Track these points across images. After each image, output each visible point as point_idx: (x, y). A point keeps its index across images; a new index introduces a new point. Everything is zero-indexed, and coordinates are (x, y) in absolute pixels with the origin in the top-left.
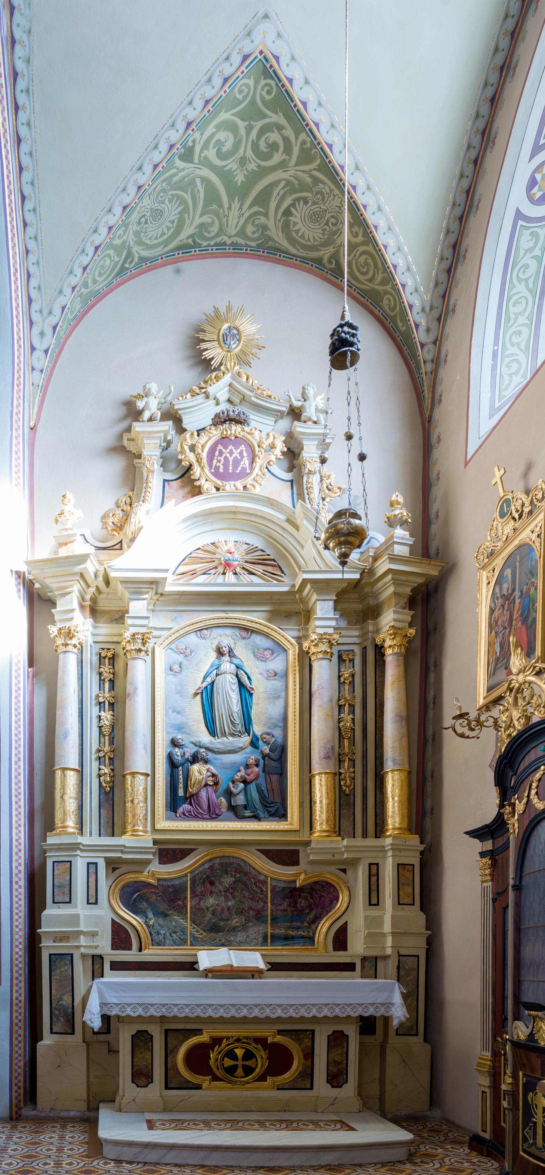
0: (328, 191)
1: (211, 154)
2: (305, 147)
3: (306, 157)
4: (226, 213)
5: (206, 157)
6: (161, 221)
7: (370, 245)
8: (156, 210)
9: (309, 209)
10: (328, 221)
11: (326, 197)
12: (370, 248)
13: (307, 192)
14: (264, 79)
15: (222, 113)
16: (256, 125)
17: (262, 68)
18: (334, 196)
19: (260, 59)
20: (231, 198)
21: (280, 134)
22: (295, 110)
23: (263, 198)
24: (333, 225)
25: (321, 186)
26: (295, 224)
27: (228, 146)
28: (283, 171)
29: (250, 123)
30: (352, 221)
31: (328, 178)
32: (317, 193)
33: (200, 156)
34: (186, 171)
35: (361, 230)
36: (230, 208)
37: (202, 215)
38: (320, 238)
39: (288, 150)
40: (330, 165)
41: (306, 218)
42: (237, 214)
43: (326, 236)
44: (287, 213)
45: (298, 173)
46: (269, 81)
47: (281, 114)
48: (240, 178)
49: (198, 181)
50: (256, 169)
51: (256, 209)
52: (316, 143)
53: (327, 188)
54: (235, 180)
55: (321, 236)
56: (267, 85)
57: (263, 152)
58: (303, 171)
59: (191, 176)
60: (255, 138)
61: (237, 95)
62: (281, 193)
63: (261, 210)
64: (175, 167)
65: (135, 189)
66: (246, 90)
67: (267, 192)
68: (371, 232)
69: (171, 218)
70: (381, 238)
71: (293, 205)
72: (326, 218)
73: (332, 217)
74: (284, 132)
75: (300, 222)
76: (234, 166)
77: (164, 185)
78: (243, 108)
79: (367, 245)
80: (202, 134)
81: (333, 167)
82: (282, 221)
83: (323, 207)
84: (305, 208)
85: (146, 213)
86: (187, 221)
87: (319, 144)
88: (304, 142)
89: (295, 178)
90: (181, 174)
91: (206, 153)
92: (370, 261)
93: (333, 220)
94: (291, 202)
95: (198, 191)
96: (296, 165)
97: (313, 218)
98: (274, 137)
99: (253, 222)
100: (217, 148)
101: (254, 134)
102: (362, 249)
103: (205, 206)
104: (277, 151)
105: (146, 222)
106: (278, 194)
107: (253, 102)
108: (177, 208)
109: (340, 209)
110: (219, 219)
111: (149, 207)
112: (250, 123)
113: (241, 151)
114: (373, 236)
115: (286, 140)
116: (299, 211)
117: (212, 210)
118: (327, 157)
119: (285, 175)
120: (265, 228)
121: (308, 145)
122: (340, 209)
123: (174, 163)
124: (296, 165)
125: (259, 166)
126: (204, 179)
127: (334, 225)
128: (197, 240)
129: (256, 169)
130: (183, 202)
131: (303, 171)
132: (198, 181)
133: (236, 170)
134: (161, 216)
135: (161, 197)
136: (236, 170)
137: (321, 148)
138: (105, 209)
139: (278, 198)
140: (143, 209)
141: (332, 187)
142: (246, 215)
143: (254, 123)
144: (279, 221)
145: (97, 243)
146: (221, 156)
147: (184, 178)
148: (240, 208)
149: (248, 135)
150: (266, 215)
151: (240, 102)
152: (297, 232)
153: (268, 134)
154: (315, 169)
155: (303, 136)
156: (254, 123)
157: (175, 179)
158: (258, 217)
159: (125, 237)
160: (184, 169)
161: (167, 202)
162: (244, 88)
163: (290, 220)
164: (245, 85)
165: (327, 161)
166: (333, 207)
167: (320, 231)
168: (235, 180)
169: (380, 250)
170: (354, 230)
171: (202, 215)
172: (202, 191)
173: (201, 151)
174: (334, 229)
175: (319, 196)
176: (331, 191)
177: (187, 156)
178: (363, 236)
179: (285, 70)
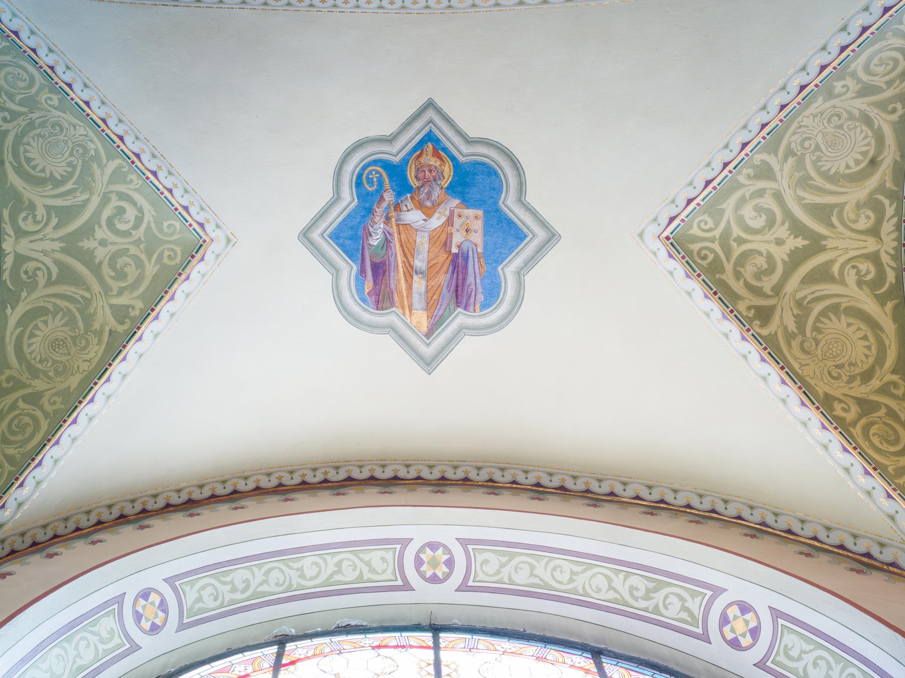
3: (121, 313)
23: (67, 276)
29: (143, 242)
36: (53, 240)
37: (45, 206)
48: (87, 244)
49: (85, 197)
51: (55, 270)
53: (96, 348)
62: (77, 297)
80: (136, 190)
92: (29, 430)
101: (133, 250)
102: (39, 414)
108: (831, 320)
112: (143, 242)
115: (134, 286)
120: (859, 206)
124: (111, 307)
125: (100, 263)
128: (876, 292)
143: (142, 247)
148: (53, 251)
150: (49, 283)
152: (36, 327)
157: (95, 166)
174: (845, 115)
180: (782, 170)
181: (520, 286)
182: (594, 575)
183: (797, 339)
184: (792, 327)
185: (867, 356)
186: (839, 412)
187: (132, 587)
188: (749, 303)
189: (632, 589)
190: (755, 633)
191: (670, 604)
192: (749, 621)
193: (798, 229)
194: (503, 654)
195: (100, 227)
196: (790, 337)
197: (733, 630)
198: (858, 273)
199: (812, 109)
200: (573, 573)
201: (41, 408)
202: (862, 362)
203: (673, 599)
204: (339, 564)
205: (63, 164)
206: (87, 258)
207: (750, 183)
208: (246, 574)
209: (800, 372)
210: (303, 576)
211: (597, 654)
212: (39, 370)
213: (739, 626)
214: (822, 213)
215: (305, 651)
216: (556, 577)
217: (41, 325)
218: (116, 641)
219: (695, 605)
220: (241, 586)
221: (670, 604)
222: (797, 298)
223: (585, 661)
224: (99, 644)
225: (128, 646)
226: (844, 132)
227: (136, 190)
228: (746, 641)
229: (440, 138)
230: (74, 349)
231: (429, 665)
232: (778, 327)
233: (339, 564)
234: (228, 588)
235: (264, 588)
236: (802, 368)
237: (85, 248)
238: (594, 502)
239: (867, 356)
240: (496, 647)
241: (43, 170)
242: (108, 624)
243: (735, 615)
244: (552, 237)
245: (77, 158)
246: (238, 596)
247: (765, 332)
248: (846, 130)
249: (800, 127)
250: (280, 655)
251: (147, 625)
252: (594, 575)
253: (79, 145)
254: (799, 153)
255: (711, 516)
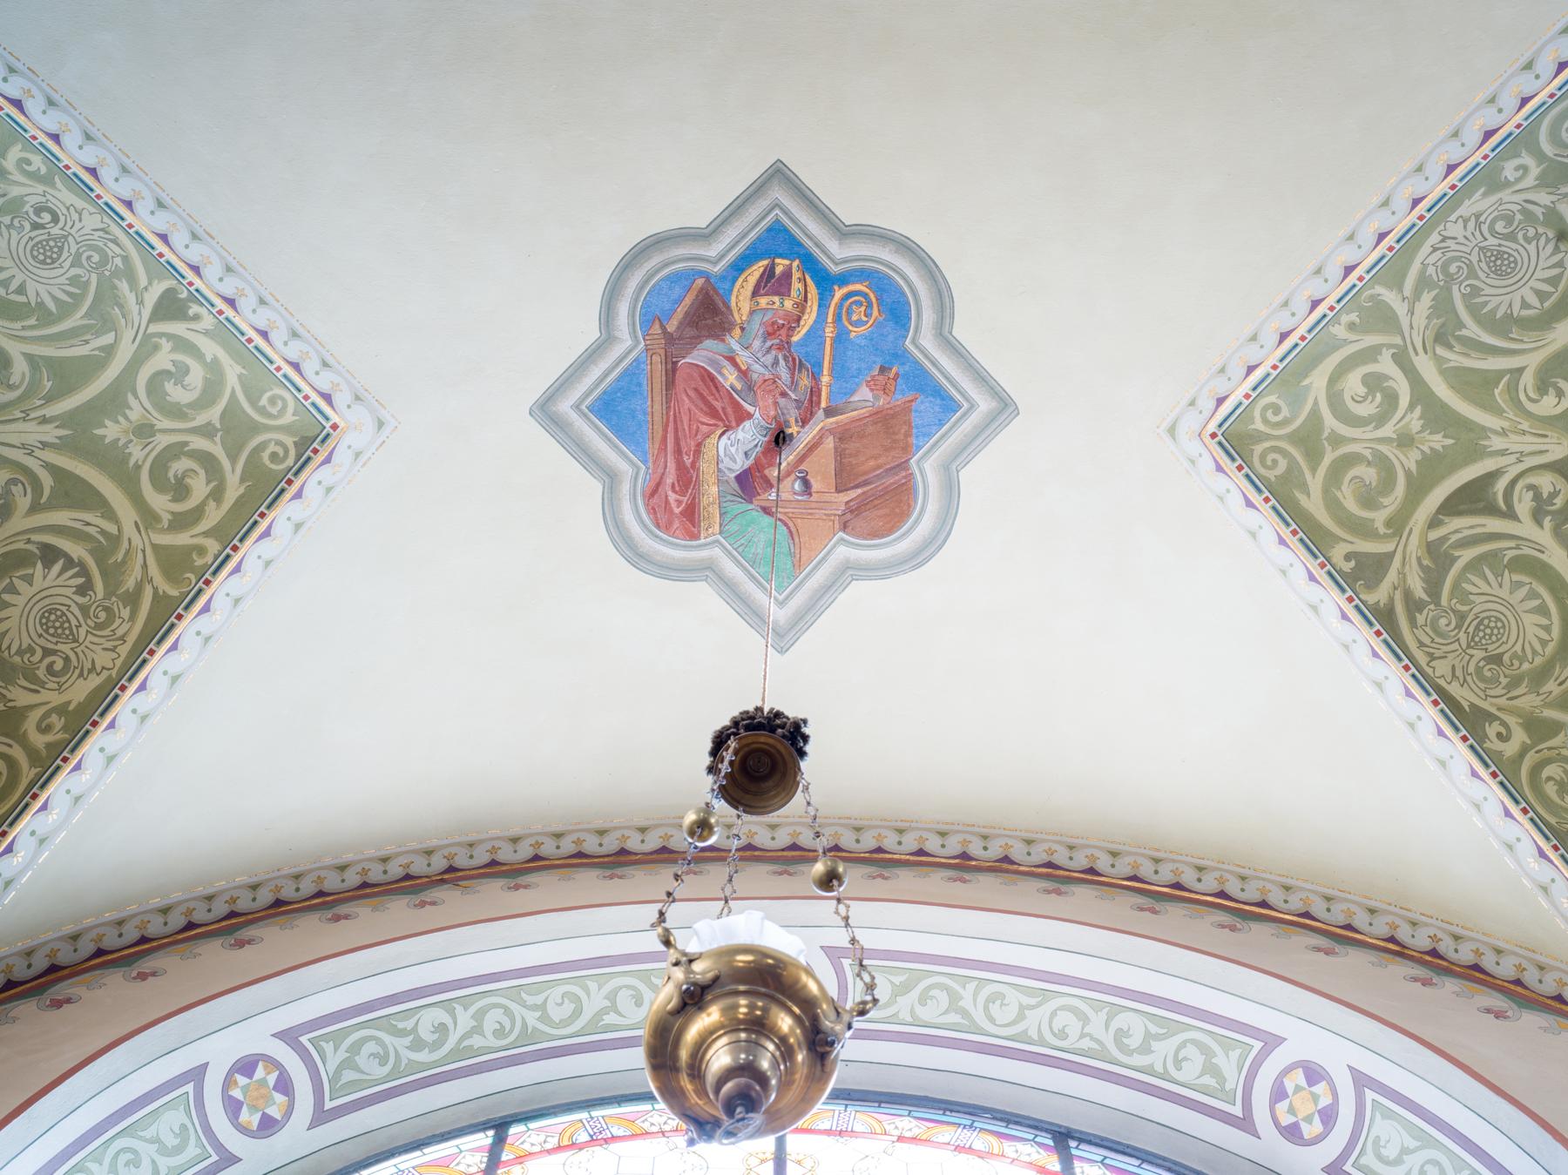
0: (120, 632)
1: (163, 359)
2: (195, 557)
3: (176, 562)
4: (33, 415)
5: (156, 348)
6: (30, 263)
7: (34, 771)
8: (61, 249)
9: (68, 602)
10: (54, 652)
11: (107, 632)
12: (28, 773)
13: (106, 586)
14: (295, 443)
15: (239, 369)
16: (215, 443)
17: (310, 434)
18: (113, 650)
19: (325, 428)
20: (65, 420)
21: (207, 498)
22: (256, 517)
23: (73, 492)
24: (50, 667)
25: (126, 613)
26: (29, 580)
27: (177, 394)
28: (136, 522)
29: (218, 430)
30: (71, 708)
31: (145, 624)
32: (106, 609)
33: (161, 335)
34: (135, 309)
35: (60, 736)
36: (44, 420)
37: (30, 358)
38: (9, 648)
39: (181, 522)
40: (173, 619)
41: (47, 601)
42: (31, 439)
43: (17, 659)
44: (50, 555)
45: (140, 555)
46: (292, 453)
47: (242, 490)
48: (111, 431)
49: (108, 339)
50: (131, 463)
51: (47, 481)
52: (207, 576)
53: (125, 627)
54: (107, 422)
55: (13, 651)
56: (286, 451)
57: (166, 469)
58: (145, 566)
59: (123, 321)
60: (192, 446)
61: (268, 394)
63: (47, 492)
64: (150, 283)
65: (127, 196)
66: (274, 411)
67: (86, 497)
68: (65, 760)
69: (31, 288)
70: (60, 788)
71: (70, 562)
72: (60, 647)
73: (67, 659)
74: (212, 504)
75: (35, 589)
76: (135, 414)
77: (118, 261)
78: (244, 412)
79: (33, 764)
80: (206, 333)
81: (173, 626)
82: (29, 547)
83: (82, 631)
84: (69, 592)
85: (61, 224)
86: (18, 325)
87: (207, 583)
88: (201, 550)
89: (128, 552)
90: (131, 298)
91: (166, 346)
93: (59, 665)
94: (75, 557)
95: (87, 342)
96: (155, 547)
97: (53, 617)
98: (200, 487)
99: (14, 481)
100: (173, 369)
101: (199, 443)
102: (17, 752)
103: (50, 361)
104: (175, 500)
105: (36, 226)
106: (88, 524)
107: (256, 428)
108: (54, 298)
109: (90, 671)
110: (20, 399)
111: (73, 231)
112: (218, 430)
113: (166, 423)
114: (58, 768)
115: (197, 513)
116: (60, 581)
117: (41, 380)
118: (186, 608)
119: (129, 530)
121: (199, 562)
122: (90, 671)
123: (160, 280)
125: (138, 467)
126: (109, 350)
127: (50, 669)
129: (131, 463)
130: (65, 310)
131: (145, 566)
132: (108, 339)
133: (127, 418)
134: (43, 262)
135: (89, 258)
136: (127, 418)
137: (200, 591)
138: (89, 126)
139: (78, 525)
140: (75, 216)
141: (131, 639)
142: (30, 462)
143: (218, 439)
144: (29, 541)
145: (29, 105)
146: (160, 376)
147: (121, 307)
148: (45, 445)
149: (194, 431)
151: (253, 403)
152: (1542, 295)
153: (202, 472)
154: (155, 589)
155: (213, 546)
156: (218, 439)
157: (124, 286)
158: (29, 490)
159: (22, 179)
160: (140, 303)
161: (74, 271)
162: (280, 404)
163: (34, 565)
164: (285, 407)
165: (180, 610)
166: (90, 655)
167: (26, 642)
168: (107, 422)
169: (35, 796)
170: (54, 718)
171: (30, 358)
172: (83, 351)
173: (170, 337)
174: (41, 673)
175: (103, 615)
176: (123, 639)
177: (171, 307)
178: (49, 746)
179: (314, 480)
180: (1413, 314)
181: (951, 490)
182: (1054, 1014)
183: (1425, 612)
184: (1418, 589)
185: (1544, 643)
186: (1494, 744)
187: (220, 1052)
188: (1349, 548)
189: (1120, 1034)
190: (1328, 1116)
191: (1185, 1059)
192: (1319, 1096)
193: (1438, 416)
194: (898, 1141)
195: (1408, 473)
196: (1414, 606)
197: (1292, 1110)
198: (1537, 497)
199: (1466, 209)
200: (1022, 1008)
201: (23, 741)
202: (1534, 652)
203: (1191, 1051)
204: (612, 996)
205: (63, 280)
206: (114, 461)
207: (1354, 337)
208: (440, 1015)
209: (1429, 671)
210: (545, 1019)
211: (1063, 1138)
212: (13, 667)
213: (1303, 1105)
214: (1477, 386)
215: (542, 1137)
216: (992, 1012)
217: (1533, 300)
218: (192, 1151)
219: (1230, 1068)
220: (426, 1033)
221: (1185, 1059)
222: (1429, 540)
223: (1035, 1153)
224: (158, 1158)
225: (215, 1158)
226: (1519, 247)
227: (206, 333)
228: (1311, 1129)
229: (766, 227)
230: (1474, 258)
231: (763, 1161)
232: (1395, 588)
233: (612, 996)
234: (407, 1041)
235: (477, 1041)
236: (1433, 664)
237: (107, 441)
238: (1056, 885)
239: (1544, 643)
240: (887, 1127)
241: (1516, 586)
242: (170, 1122)
243: (1297, 1085)
244: (1005, 406)
245: (88, 271)
246: (423, 1056)
247: (1371, 598)
248: (1522, 242)
249: (1444, 239)
250: (500, 1141)
251: (250, 1118)
252: (1054, 1014)
253: (91, 247)
254: (114, 599)
255: (1258, 911)
